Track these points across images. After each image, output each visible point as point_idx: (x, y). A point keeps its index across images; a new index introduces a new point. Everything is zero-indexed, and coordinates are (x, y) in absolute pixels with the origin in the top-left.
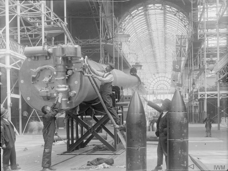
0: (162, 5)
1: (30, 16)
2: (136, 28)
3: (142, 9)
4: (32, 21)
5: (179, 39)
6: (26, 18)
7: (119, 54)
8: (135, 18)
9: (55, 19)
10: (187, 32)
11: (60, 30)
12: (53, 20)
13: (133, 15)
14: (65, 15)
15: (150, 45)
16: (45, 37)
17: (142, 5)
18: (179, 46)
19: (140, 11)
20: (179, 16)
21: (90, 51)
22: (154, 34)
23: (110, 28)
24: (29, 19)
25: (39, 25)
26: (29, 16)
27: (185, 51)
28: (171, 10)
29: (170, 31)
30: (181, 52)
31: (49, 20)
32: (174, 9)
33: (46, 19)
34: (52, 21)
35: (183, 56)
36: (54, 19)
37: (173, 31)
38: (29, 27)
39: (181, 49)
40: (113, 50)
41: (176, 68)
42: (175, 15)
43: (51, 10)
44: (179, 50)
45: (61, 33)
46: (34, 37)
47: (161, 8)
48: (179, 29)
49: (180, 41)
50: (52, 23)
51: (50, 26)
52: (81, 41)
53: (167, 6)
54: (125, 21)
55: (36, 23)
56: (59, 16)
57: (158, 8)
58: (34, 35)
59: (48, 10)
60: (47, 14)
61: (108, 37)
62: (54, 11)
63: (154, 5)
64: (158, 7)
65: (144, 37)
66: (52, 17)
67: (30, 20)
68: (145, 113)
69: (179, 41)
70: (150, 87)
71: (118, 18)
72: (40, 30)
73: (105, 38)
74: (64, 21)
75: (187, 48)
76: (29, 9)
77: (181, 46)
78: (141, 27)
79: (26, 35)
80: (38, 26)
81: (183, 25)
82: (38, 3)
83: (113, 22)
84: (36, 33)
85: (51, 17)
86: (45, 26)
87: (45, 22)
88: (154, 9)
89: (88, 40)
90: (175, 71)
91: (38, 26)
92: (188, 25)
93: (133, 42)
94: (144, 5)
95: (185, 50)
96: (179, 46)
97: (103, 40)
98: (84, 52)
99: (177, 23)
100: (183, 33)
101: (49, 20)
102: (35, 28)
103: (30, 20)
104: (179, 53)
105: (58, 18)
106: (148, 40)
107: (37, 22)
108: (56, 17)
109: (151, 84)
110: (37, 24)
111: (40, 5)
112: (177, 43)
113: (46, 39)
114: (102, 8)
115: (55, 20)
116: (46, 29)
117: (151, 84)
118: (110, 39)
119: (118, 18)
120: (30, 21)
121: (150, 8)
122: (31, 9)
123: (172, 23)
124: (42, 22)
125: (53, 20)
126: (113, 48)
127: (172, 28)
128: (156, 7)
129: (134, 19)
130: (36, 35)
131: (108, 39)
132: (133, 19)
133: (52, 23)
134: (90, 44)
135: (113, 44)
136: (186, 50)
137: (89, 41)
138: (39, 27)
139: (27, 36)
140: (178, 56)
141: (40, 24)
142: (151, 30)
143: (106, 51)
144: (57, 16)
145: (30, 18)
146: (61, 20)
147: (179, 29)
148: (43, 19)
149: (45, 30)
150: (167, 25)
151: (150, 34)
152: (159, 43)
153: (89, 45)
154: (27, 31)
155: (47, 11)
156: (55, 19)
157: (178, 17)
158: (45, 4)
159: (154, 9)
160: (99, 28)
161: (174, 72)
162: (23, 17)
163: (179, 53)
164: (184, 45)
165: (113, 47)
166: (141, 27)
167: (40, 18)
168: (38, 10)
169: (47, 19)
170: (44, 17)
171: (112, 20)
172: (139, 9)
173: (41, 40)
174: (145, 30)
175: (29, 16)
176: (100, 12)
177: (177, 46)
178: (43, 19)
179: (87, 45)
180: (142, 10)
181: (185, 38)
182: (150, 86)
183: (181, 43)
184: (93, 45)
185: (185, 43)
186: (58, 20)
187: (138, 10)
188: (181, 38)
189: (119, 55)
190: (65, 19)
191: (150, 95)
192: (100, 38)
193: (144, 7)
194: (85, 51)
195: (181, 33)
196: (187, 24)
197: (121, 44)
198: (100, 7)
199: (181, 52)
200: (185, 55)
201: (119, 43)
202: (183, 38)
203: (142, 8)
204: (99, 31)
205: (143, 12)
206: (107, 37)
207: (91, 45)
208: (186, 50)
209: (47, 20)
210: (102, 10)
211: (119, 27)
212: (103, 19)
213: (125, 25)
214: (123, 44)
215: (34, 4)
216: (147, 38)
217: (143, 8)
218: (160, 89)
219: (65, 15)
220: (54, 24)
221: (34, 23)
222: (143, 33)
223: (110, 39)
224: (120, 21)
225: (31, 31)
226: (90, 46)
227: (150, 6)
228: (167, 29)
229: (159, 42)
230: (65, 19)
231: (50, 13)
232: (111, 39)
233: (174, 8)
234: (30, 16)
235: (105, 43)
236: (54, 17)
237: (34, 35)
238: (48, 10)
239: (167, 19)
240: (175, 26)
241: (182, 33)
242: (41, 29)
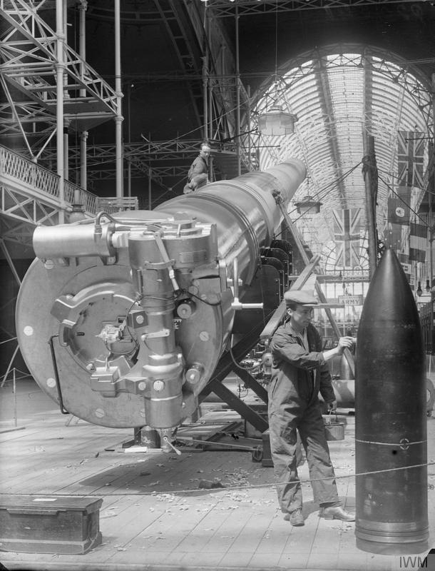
0: (362, 57)
1: (25, 72)
2: (291, 102)
3: (310, 65)
4: (31, 86)
5: (406, 139)
6: (14, 78)
7: (242, 164)
8: (292, 88)
9: (91, 81)
10: (427, 124)
11: (104, 113)
12: (86, 83)
13: (288, 82)
14: (118, 72)
15: (330, 158)
16: (65, 130)
17: (311, 55)
18: (406, 159)
19: (306, 71)
20: (406, 83)
21: (171, 171)
22: (341, 128)
23: (229, 113)
24: (23, 81)
25: (49, 97)
26: (22, 74)
27: (421, 173)
28: (384, 68)
29: (380, 121)
30: (410, 175)
31: (77, 83)
32: (395, 68)
33: (66, 82)
34: (83, 86)
35: (416, 185)
36: (89, 83)
37: (388, 122)
38: (23, 105)
39: (411, 166)
40: (237, 167)
41: (397, 213)
42: (395, 80)
43: (82, 58)
44: (407, 168)
45: (108, 118)
46: (36, 131)
47: (358, 62)
48: (404, 116)
49: (407, 145)
50: (83, 93)
51: (77, 101)
52: (153, 144)
53: (374, 58)
54: (267, 95)
55: (41, 91)
56: (102, 74)
57: (351, 64)
58: (34, 124)
59: (74, 59)
60: (70, 67)
61: (225, 137)
62: (89, 60)
63: (341, 56)
64: (351, 61)
65: (313, 138)
66: (83, 76)
67: (26, 84)
68: (336, 108)
69: (406, 146)
70: (326, 263)
71: (249, 88)
72: (52, 111)
73: (217, 138)
74: (114, 87)
75: (426, 162)
76: (24, 54)
77: (410, 159)
78: (308, 113)
79: (16, 125)
80: (45, 100)
81: (416, 108)
82: (48, 38)
83: (236, 98)
84: (41, 119)
85: (81, 76)
86: (64, 101)
87: (65, 89)
88: (341, 66)
89: (173, 143)
90: (392, 223)
91: (45, 100)
92: (428, 107)
93: (287, 149)
94: (314, 56)
95: (420, 168)
96: (406, 159)
97: (212, 142)
98: (162, 174)
99: (399, 113)
100: (418, 123)
101: (78, 85)
102: (39, 106)
103: (26, 84)
104: (405, 177)
105: (99, 80)
106: (324, 153)
107: (45, 90)
108: (95, 78)
109: (328, 257)
110: (45, 93)
111: (53, 45)
112: (401, 150)
113: (67, 135)
114: (211, 63)
115: (91, 85)
116: (67, 109)
117: (328, 257)
118: (229, 139)
119: (249, 88)
120: (27, 87)
121: (331, 63)
122: (30, 53)
123: (387, 89)
124: (58, 89)
125: (86, 83)
126: (237, 164)
127: (386, 114)
128: (345, 61)
129: (291, 90)
130: (42, 126)
131: (224, 141)
132: (287, 91)
133: (83, 93)
134: (177, 151)
135: (238, 152)
136: (425, 170)
137: (176, 144)
138: (49, 104)
139: (18, 127)
140: (404, 185)
141: (52, 95)
142: (333, 119)
143: (219, 171)
144: (95, 73)
145: (26, 78)
146: (107, 86)
147: (404, 116)
148: (61, 81)
149: (64, 112)
150: (373, 107)
151: (331, 130)
152: (351, 152)
153: (176, 154)
154: (19, 116)
155: (70, 59)
156: (91, 81)
157: (403, 84)
158: (66, 42)
159: (341, 66)
160: (202, 112)
161: (390, 224)
162: (9, 76)
163: (405, 177)
164: (418, 157)
165: (237, 160)
166: (308, 113)
167: (52, 80)
168: (46, 57)
169: (71, 80)
170: (64, 77)
171: (236, 94)
172: (303, 65)
173: (55, 138)
174: (316, 120)
175: (22, 74)
176: (206, 73)
177: (400, 158)
178: (61, 81)
179: (170, 157)
180: (311, 68)
181: (421, 137)
182: (328, 262)
183: (411, 151)
184: (186, 156)
185: (420, 151)
186: (105, 96)
187: (301, 69)
188: (409, 138)
189: (242, 167)
190: (118, 82)
191: (328, 284)
192: (204, 136)
193: (316, 60)
194: (163, 172)
195: (412, 123)
196: (425, 103)
197: (257, 154)
198: (205, 59)
199: (410, 175)
200: (422, 183)
201: (253, 151)
202: (417, 139)
203: (310, 62)
204: (202, 120)
205: (312, 73)
206: (222, 136)
207: (180, 155)
208: (425, 170)
209: (68, 84)
210: (210, 68)
211: (252, 111)
212: (211, 89)
213: (266, 107)
214: (263, 151)
215: (36, 39)
216: (322, 139)
217: (313, 64)
218: (353, 270)
219: (118, 72)
220: (88, 94)
221: (35, 92)
222: (313, 126)
223: (229, 139)
224: (254, 97)
225: (28, 114)
226: (179, 158)
227: (329, 57)
228: (373, 131)
229: (352, 151)
230: (118, 82)
231: (78, 66)
232: (232, 141)
233: (392, 62)
234: (25, 72)
235: (216, 151)
236: (88, 76)
237: (34, 124)
238: (74, 59)
239: (373, 91)
240: (392, 109)
241: (414, 125)
242: (55, 107)
